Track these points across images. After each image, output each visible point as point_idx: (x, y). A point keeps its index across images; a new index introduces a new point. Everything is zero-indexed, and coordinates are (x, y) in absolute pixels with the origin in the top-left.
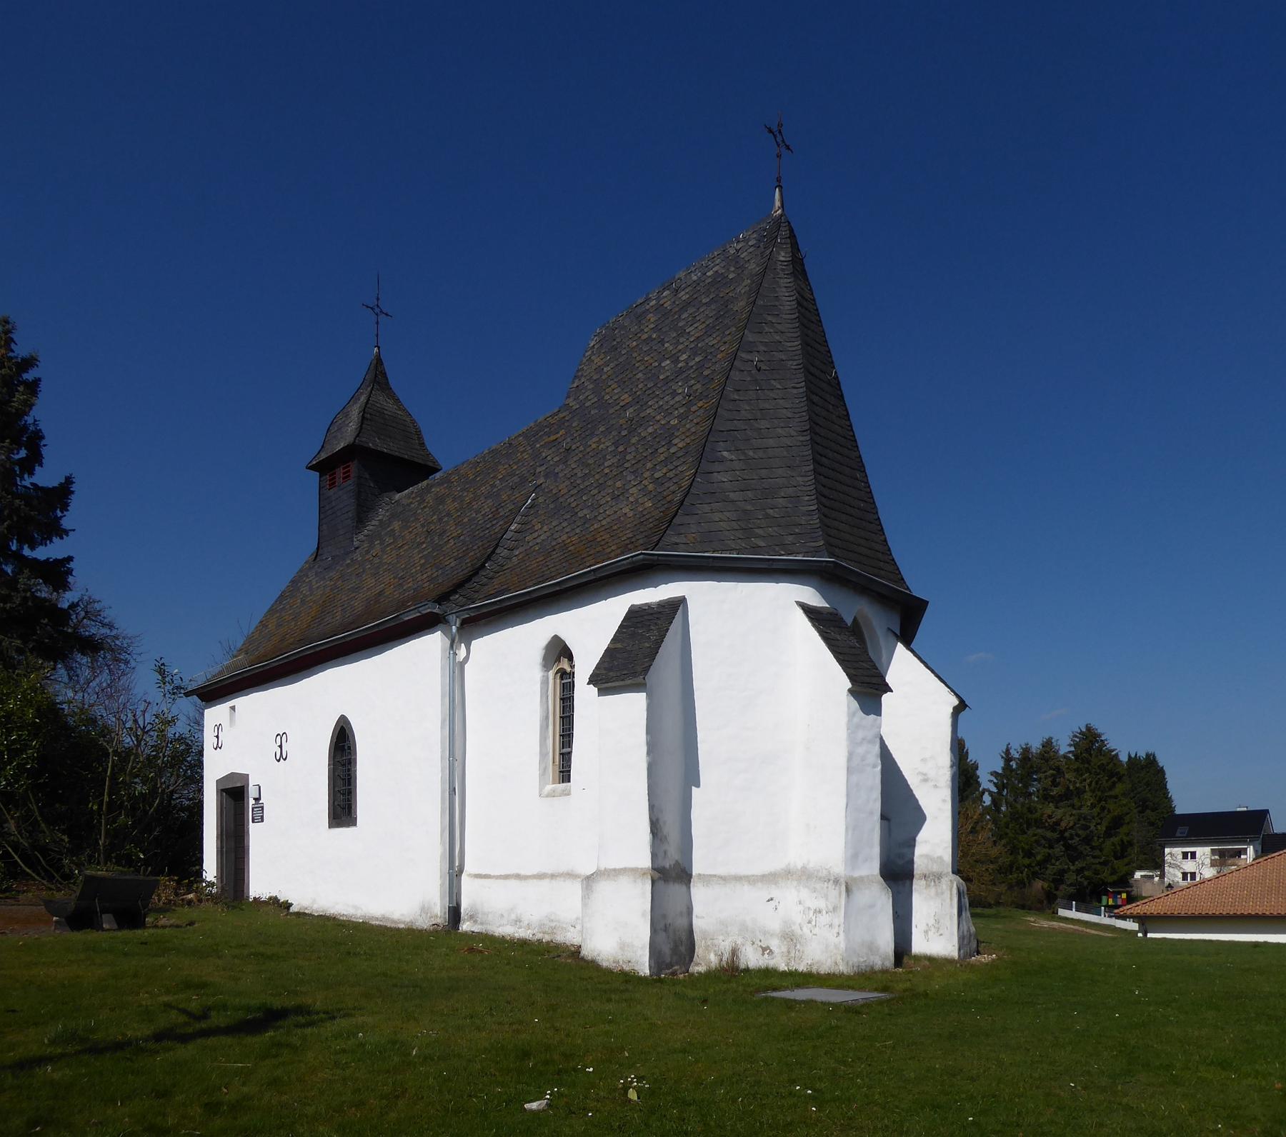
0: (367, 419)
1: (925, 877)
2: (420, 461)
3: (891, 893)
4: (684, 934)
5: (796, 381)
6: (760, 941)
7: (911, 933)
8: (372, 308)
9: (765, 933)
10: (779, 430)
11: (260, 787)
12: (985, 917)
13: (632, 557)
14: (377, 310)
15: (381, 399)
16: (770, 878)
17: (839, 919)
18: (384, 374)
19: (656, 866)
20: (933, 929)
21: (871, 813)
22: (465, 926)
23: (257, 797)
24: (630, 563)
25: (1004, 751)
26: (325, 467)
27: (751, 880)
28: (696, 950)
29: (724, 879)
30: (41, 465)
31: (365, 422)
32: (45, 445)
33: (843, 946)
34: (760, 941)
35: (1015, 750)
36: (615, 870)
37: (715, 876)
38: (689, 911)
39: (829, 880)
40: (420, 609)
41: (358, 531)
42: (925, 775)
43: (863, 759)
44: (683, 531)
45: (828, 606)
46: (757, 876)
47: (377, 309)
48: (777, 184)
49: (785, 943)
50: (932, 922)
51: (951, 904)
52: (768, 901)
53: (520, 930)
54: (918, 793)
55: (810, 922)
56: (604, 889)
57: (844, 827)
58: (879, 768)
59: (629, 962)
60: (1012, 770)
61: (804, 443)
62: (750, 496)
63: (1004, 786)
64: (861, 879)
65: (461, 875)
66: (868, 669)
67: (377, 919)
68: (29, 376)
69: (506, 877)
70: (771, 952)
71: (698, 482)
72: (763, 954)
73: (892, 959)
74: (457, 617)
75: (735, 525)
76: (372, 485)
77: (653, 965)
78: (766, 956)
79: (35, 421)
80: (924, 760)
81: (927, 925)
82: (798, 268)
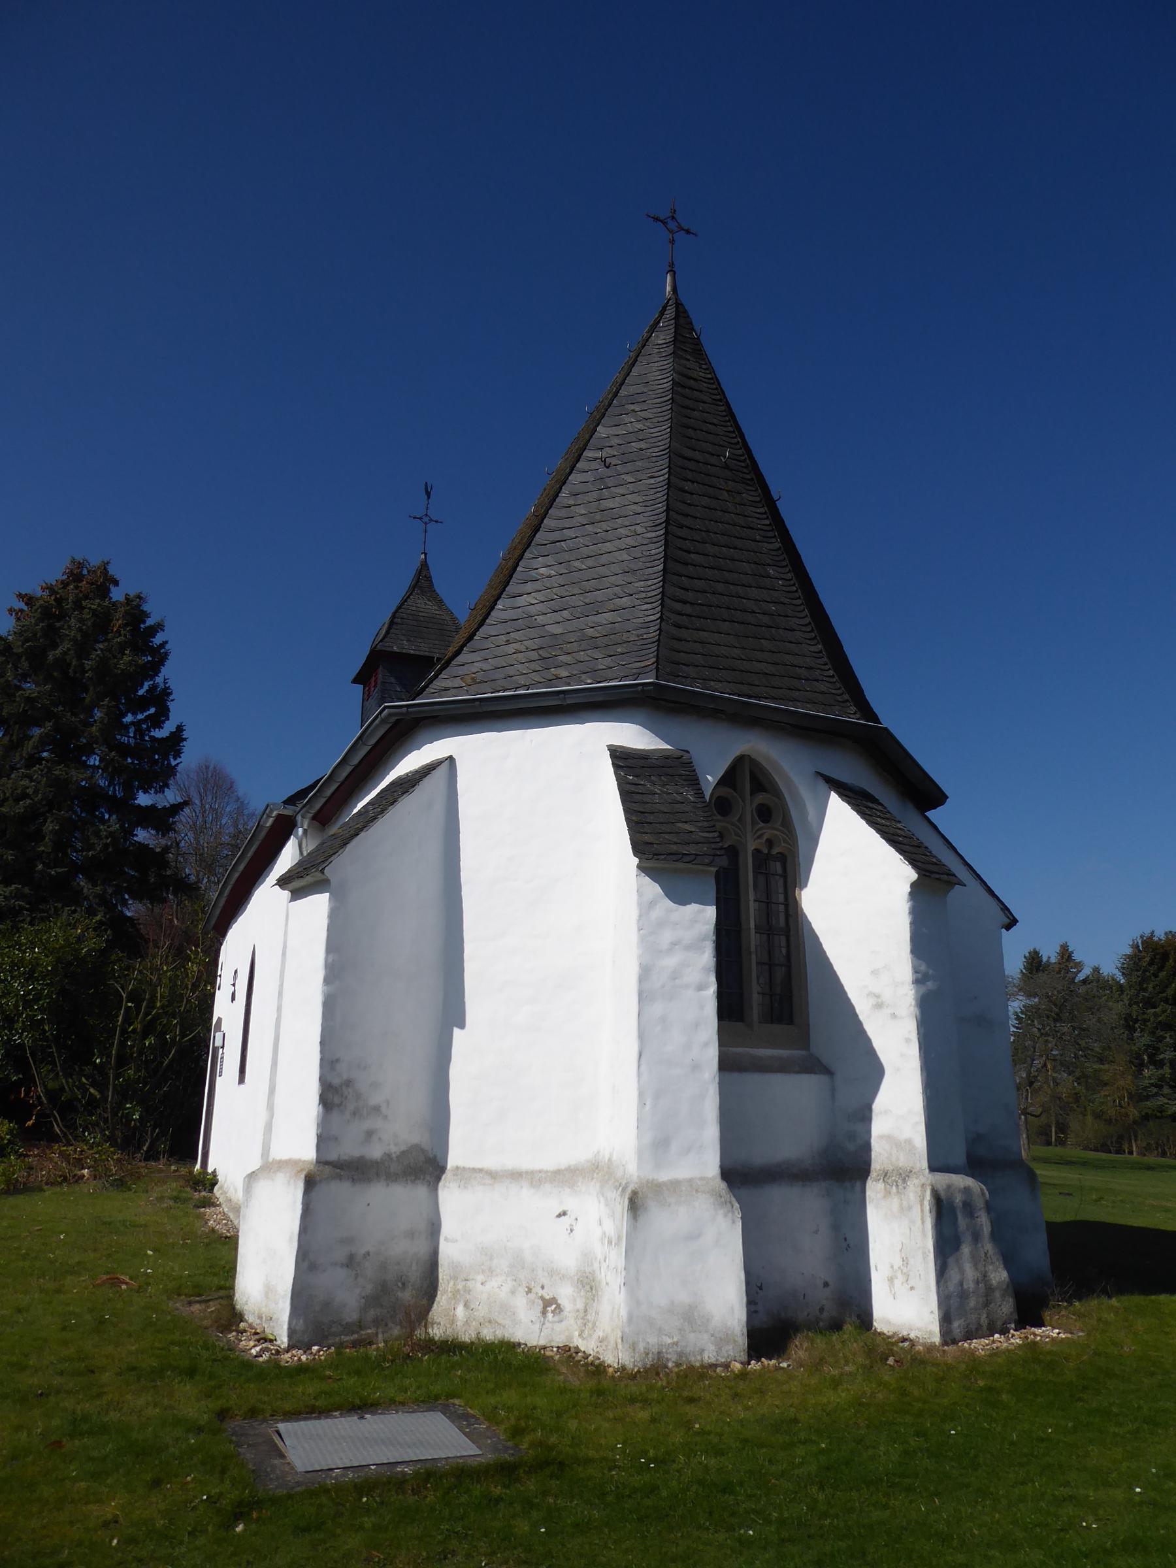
1: (886, 1175)
3: (737, 1205)
4: (414, 1267)
6: (543, 1287)
7: (870, 1281)
9: (552, 1273)
11: (224, 1034)
18: (429, 579)
19: (333, 1157)
20: (899, 1274)
21: (696, 1067)
28: (437, 1299)
29: (494, 1176)
32: (172, 700)
34: (543, 1287)
37: (481, 1170)
38: (434, 1228)
42: (878, 996)
45: (669, 747)
48: (669, 269)
49: (582, 1293)
50: (898, 1262)
52: (559, 1216)
54: (870, 1028)
58: (712, 989)
62: (565, 616)
64: (675, 1185)
70: (559, 1309)
73: (742, 1341)
75: (534, 655)
76: (399, 690)
77: (300, 1325)
79: (165, 680)
80: (875, 973)
81: (892, 1267)
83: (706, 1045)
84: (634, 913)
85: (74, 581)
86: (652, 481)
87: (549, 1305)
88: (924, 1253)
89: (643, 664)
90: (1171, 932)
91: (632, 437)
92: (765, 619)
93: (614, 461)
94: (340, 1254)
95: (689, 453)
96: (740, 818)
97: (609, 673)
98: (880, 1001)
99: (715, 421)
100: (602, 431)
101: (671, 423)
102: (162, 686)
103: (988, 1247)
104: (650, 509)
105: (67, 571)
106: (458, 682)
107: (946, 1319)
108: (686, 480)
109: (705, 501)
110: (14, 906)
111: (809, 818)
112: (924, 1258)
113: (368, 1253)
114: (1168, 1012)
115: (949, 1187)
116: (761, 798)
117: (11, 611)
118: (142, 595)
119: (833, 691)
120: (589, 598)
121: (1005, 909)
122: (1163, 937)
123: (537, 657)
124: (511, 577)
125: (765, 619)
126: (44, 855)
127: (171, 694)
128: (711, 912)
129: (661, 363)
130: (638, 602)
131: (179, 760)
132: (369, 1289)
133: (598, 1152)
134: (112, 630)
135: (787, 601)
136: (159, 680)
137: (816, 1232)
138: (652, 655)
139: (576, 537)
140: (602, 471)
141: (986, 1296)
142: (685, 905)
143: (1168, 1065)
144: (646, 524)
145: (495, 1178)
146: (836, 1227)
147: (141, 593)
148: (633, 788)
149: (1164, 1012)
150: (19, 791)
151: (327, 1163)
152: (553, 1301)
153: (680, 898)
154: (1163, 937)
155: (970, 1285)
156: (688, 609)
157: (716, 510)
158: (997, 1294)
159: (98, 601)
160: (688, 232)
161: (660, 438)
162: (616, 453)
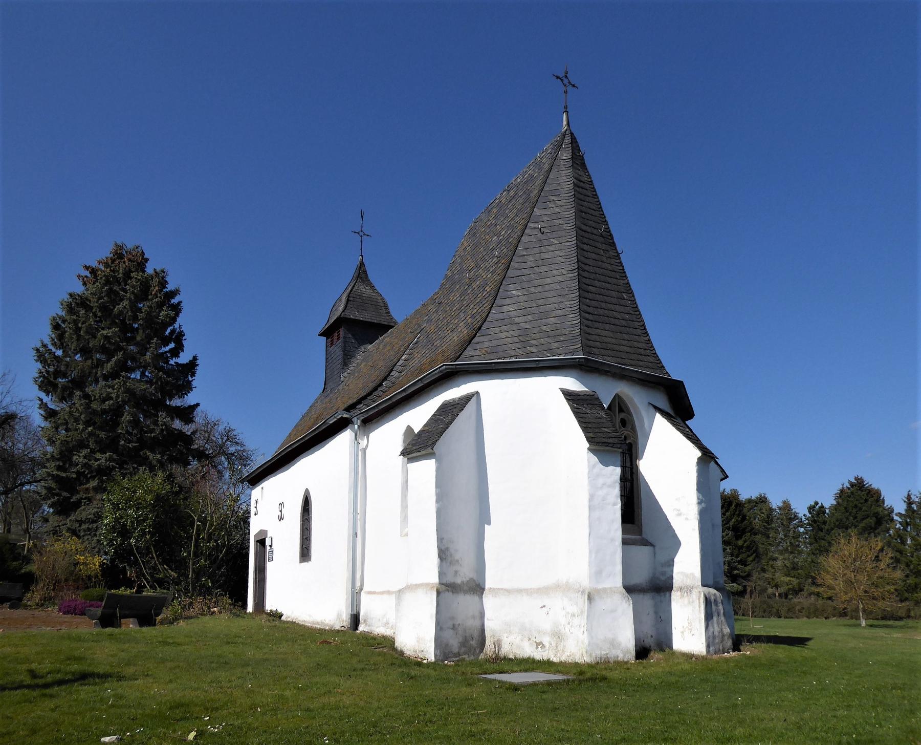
0: (351, 301)
1: (681, 589)
2: (386, 323)
3: (630, 598)
5: (569, 237)
6: (535, 638)
8: (358, 233)
9: (539, 632)
10: (554, 272)
12: (894, 627)
13: (439, 368)
14: (361, 234)
15: (362, 288)
16: (544, 591)
17: (584, 621)
18: (365, 272)
19: (444, 582)
20: (687, 629)
22: (362, 628)
23: (271, 544)
24: (438, 373)
25: (906, 496)
26: (327, 333)
27: (528, 592)
29: (508, 591)
30: (183, 351)
31: (349, 302)
32: (185, 339)
33: (586, 642)
34: (535, 638)
35: (915, 495)
36: (416, 585)
37: (502, 589)
38: (482, 615)
39: (579, 591)
40: (335, 415)
41: (343, 371)
42: (679, 510)
43: (604, 499)
44: (478, 347)
45: (587, 390)
46: (534, 589)
47: (361, 234)
51: (700, 610)
52: (542, 607)
53: (387, 630)
55: (569, 624)
56: (408, 597)
57: (588, 551)
59: (423, 651)
60: (914, 511)
61: (573, 278)
62: (529, 318)
63: (907, 524)
64: (605, 590)
65: (360, 592)
66: (609, 432)
67: (318, 624)
68: (174, 301)
69: (382, 593)
70: (544, 646)
71: (493, 313)
72: (537, 648)
73: (634, 653)
74: (358, 419)
75: (516, 339)
76: (354, 342)
77: (438, 653)
78: (539, 649)
79: (180, 326)
81: (683, 627)
82: (578, 161)
83: (617, 530)
84: (587, 471)
85: (118, 258)
86: (568, 244)
87: (539, 644)
88: (700, 620)
89: (575, 347)
90: (734, 490)
91: (554, 217)
92: (624, 323)
93: (546, 230)
94: (450, 624)
95: (584, 228)
96: (632, 427)
97: (559, 351)
98: (680, 512)
99: (594, 208)
100: (537, 212)
101: (575, 209)
102: (178, 330)
103: (723, 618)
104: (569, 260)
105: (113, 251)
106: (477, 353)
107: (708, 646)
108: (585, 244)
109: (593, 256)
110: (109, 466)
111: (645, 426)
112: (699, 622)
113: (459, 624)
114: (730, 535)
115: (709, 593)
116: (623, 415)
117: (79, 276)
118: (165, 270)
119: (656, 362)
120: (542, 309)
121: (723, 471)
122: (729, 492)
123: (518, 341)
124: (497, 295)
125: (624, 323)
126: (121, 435)
127: (184, 335)
128: (618, 470)
129: (566, 172)
130: (568, 313)
131: (194, 378)
132: (461, 640)
133: (558, 580)
134: (151, 293)
135: (633, 313)
136: (176, 325)
137: (648, 614)
138: (579, 342)
139: (530, 274)
140: (539, 235)
141: (722, 638)
142: (607, 467)
143: (727, 564)
144: (568, 269)
145: (510, 592)
146: (656, 613)
147: (164, 269)
148: (578, 411)
149: (727, 535)
150: (104, 395)
151: (443, 584)
152: (541, 643)
153: (605, 463)
154: (729, 492)
155: (716, 633)
156: (590, 317)
157: (598, 261)
158: (726, 638)
159: (141, 273)
160: (574, 86)
161: (570, 218)
162: (546, 226)
